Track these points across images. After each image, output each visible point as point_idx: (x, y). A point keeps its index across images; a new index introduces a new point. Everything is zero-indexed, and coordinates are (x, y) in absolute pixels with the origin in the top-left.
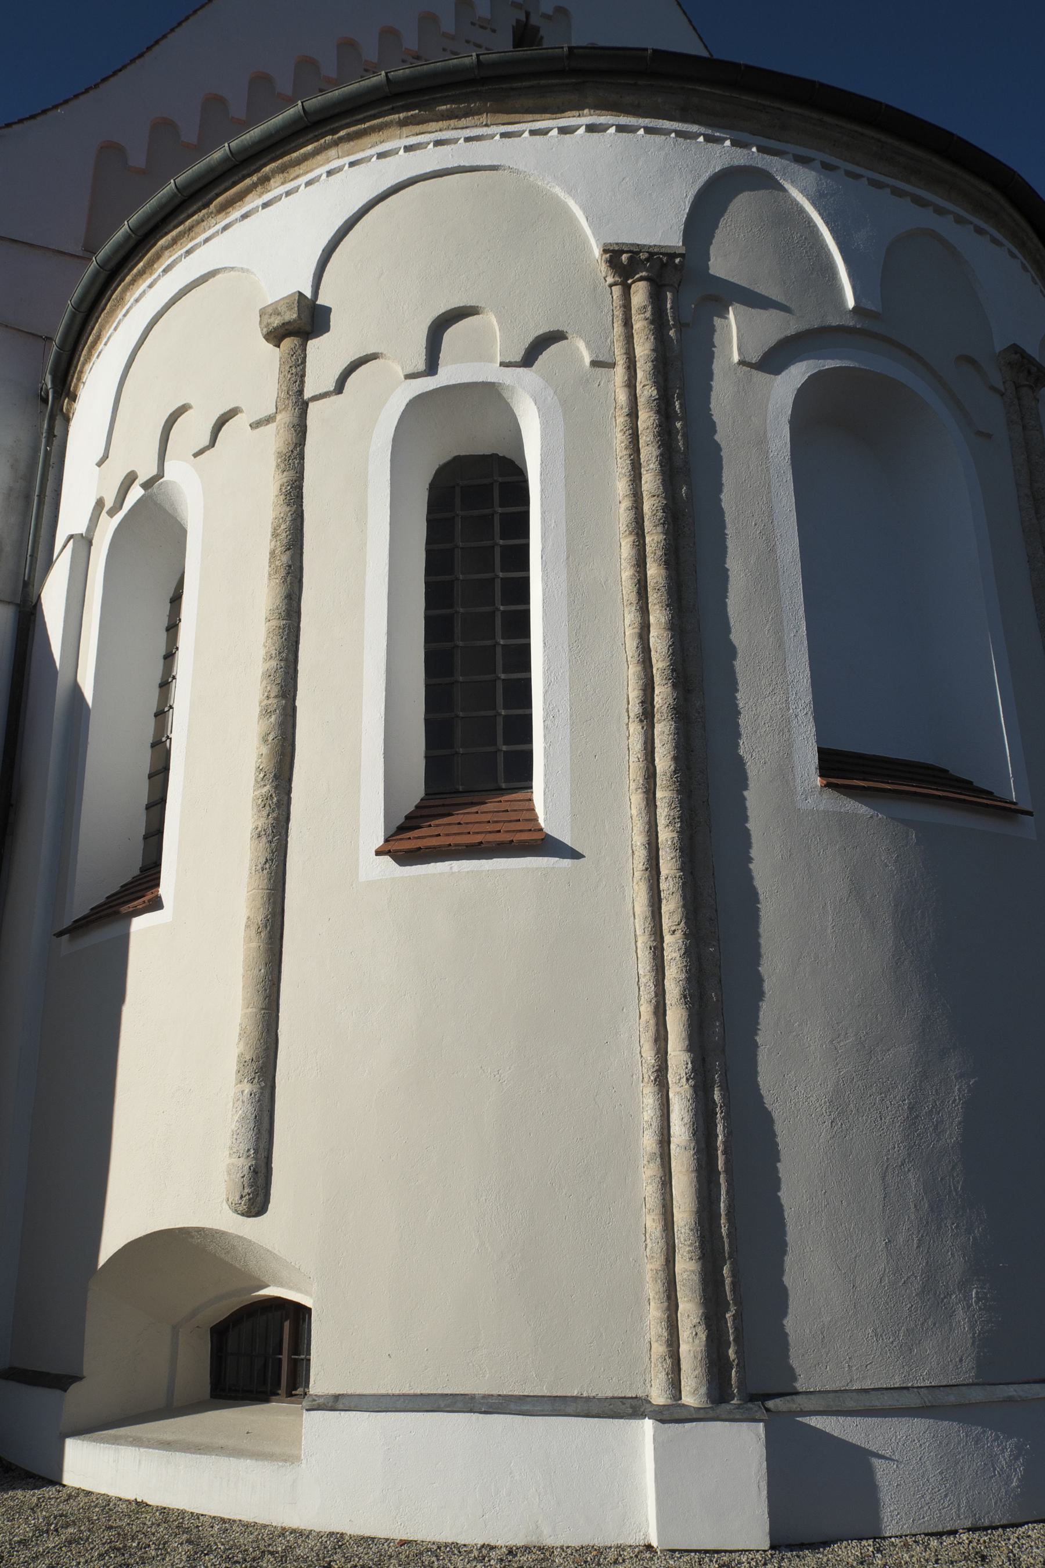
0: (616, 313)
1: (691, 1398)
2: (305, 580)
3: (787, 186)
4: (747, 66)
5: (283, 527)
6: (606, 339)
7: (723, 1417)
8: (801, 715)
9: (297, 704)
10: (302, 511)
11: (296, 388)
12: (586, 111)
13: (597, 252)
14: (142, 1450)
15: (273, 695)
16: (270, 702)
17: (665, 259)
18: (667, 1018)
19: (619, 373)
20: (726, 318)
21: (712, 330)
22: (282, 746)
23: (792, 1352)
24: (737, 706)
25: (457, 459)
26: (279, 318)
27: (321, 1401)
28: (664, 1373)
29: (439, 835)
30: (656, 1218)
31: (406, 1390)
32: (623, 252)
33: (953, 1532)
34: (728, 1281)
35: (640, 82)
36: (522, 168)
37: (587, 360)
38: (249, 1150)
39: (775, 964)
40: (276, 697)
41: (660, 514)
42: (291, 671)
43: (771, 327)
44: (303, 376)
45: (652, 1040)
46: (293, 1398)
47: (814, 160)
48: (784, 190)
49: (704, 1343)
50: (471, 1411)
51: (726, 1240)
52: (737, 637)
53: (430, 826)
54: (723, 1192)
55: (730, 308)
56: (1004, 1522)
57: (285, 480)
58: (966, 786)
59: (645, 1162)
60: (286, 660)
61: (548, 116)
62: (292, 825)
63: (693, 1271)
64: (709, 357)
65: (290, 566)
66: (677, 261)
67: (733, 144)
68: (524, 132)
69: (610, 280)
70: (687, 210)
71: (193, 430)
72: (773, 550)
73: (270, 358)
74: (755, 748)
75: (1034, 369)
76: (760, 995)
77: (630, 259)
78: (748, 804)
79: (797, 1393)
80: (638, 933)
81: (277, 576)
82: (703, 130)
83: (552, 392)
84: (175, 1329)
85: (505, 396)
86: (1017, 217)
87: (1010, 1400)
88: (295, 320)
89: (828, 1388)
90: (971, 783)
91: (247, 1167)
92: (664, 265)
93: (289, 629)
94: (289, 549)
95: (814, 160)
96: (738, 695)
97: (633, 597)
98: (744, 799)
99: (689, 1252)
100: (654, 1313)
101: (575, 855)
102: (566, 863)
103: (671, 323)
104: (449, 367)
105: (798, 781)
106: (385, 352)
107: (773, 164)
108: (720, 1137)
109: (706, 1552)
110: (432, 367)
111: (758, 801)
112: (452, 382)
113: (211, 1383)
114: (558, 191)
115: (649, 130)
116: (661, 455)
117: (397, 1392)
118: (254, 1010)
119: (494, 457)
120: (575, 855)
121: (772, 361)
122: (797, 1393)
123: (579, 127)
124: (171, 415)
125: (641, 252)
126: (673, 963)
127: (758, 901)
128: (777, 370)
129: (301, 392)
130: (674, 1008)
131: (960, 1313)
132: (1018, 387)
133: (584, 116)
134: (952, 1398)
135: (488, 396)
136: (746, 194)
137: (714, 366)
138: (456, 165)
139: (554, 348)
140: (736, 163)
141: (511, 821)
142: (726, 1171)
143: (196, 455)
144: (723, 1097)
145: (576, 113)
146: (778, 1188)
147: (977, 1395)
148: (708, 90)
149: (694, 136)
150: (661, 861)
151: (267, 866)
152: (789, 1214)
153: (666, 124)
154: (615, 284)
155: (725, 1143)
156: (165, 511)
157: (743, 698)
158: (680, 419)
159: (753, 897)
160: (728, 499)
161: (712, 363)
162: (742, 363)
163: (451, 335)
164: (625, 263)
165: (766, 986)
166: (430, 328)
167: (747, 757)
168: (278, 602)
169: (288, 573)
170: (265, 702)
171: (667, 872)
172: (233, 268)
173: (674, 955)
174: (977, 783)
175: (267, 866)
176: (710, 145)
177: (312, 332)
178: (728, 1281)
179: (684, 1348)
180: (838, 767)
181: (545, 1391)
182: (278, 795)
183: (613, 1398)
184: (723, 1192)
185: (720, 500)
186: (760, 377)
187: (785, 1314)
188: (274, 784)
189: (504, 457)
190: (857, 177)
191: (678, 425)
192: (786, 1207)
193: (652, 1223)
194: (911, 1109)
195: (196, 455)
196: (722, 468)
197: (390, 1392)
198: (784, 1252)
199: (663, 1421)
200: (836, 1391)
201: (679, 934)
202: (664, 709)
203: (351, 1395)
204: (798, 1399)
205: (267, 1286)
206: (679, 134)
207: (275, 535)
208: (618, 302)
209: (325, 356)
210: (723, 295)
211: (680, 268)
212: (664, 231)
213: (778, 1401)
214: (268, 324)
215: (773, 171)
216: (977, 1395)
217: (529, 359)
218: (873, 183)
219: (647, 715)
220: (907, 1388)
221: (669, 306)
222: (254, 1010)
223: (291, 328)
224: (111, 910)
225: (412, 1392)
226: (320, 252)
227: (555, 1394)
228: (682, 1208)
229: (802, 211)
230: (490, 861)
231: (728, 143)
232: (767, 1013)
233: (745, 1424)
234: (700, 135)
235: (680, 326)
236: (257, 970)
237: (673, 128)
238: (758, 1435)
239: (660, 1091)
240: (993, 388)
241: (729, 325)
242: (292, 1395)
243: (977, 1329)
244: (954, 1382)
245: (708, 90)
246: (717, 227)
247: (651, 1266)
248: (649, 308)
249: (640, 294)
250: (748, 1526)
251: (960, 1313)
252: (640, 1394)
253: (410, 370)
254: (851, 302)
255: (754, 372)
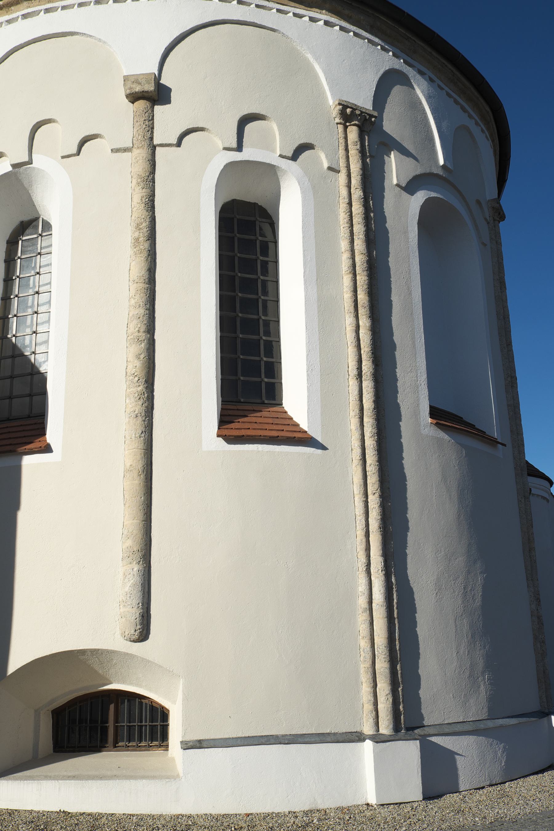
0: (341, 141)
1: (385, 729)
2: (157, 261)
3: (416, 87)
4: (408, 14)
5: (144, 224)
6: (336, 155)
7: (403, 738)
8: (423, 384)
9: (155, 338)
10: (155, 217)
11: (149, 135)
12: (324, 11)
13: (331, 101)
14: (60, 781)
15: (142, 330)
16: (140, 334)
17: (368, 117)
18: (370, 539)
19: (342, 177)
20: (390, 157)
21: (383, 163)
22: (149, 363)
23: (423, 706)
24: (396, 376)
25: (234, 201)
26: (140, 86)
27: (191, 744)
28: (372, 719)
29: (249, 429)
30: (367, 641)
31: (240, 735)
32: (348, 107)
33: (483, 788)
34: (399, 672)
35: (353, 4)
36: (289, 34)
37: (326, 165)
38: (139, 604)
39: (413, 514)
40: (144, 332)
41: (365, 264)
42: (152, 317)
43: (413, 168)
44: (153, 128)
45: (364, 549)
46: (118, 748)
47: (426, 74)
48: (414, 89)
49: (391, 703)
50: (280, 743)
51: (398, 652)
52: (397, 338)
53: (239, 422)
54: (397, 628)
55: (392, 152)
56: (500, 782)
57: (145, 194)
58: (472, 426)
59: (360, 612)
60: (149, 310)
61: (303, 7)
62: (155, 412)
63: (386, 668)
64: (383, 178)
65: (149, 251)
66: (373, 119)
67: (394, 55)
68: (289, 12)
69: (338, 120)
70: (374, 89)
71: (60, 137)
72: (410, 294)
73: (129, 111)
74: (405, 399)
75: (502, 213)
76: (407, 529)
77: (352, 112)
78: (402, 429)
79: (424, 726)
80: (355, 493)
81: (142, 255)
82: (380, 42)
83: (307, 180)
84: (37, 712)
85: (278, 174)
86: (495, 126)
87: (501, 726)
88: (151, 92)
89: (436, 723)
90: (474, 426)
91: (138, 614)
92: (366, 119)
93: (150, 290)
94: (149, 240)
95: (426, 74)
96: (397, 370)
97: (352, 309)
98: (400, 426)
99: (384, 658)
100: (366, 689)
101: (324, 448)
102: (319, 451)
103: (368, 154)
104: (249, 149)
105: (422, 419)
106: (210, 129)
107: (410, 72)
108: (395, 600)
109: (396, 804)
110: (239, 148)
111: (406, 427)
112: (251, 159)
113: (53, 744)
114: (309, 56)
115: (356, 34)
116: (366, 231)
117: (235, 736)
118: (138, 521)
119: (255, 204)
120: (324, 448)
121: (411, 187)
122: (424, 726)
123: (320, 20)
124: (37, 123)
125: (356, 109)
126: (374, 510)
127: (406, 481)
128: (412, 193)
129: (151, 139)
130: (375, 533)
131: (482, 687)
132: (494, 220)
133: (322, 14)
134: (482, 726)
135: (270, 171)
136: (396, 87)
137: (385, 184)
138: (252, 21)
139: (307, 153)
140: (395, 68)
141: (285, 425)
142: (398, 618)
143: (63, 157)
144: (396, 580)
145: (319, 11)
146: (416, 626)
147: (490, 724)
148: (385, 20)
149: (376, 44)
150: (367, 456)
151: (143, 435)
152: (421, 639)
153: (364, 33)
154: (340, 124)
155: (397, 603)
156: (22, 184)
157: (399, 372)
158: (373, 212)
159: (404, 478)
160: (392, 260)
161: (384, 182)
162: (398, 185)
163: (249, 128)
164: (348, 114)
165: (410, 524)
166: (238, 121)
167: (401, 403)
168: (143, 272)
169: (149, 255)
170: (137, 334)
171: (371, 462)
172: (91, 36)
173: (375, 506)
174: (476, 426)
175: (143, 435)
176: (383, 52)
177: (158, 100)
178: (399, 672)
179: (380, 706)
180: (434, 412)
181: (314, 732)
182: (147, 393)
183: (346, 733)
184: (397, 628)
185: (388, 261)
186: (405, 195)
187: (419, 688)
188: (145, 386)
189: (261, 206)
190: (442, 89)
191: (372, 215)
192: (419, 636)
193: (364, 644)
194: (464, 588)
195: (63, 157)
196: (389, 244)
197: (231, 736)
198: (419, 658)
199: (377, 742)
200: (439, 725)
201: (377, 495)
202: (369, 374)
203: (208, 740)
204: (425, 728)
205: (111, 683)
206: (370, 41)
207: (138, 227)
208: (341, 135)
209: (168, 120)
210: (389, 144)
211: (373, 124)
212: (364, 101)
213: (418, 730)
214: (130, 88)
215: (410, 76)
216: (490, 724)
217: (294, 157)
218: (448, 94)
219: (360, 376)
220: (464, 722)
221: (367, 144)
222: (138, 521)
223: (146, 95)
224: (8, 448)
225: (243, 736)
226: (164, 49)
227: (318, 732)
228: (381, 636)
229: (421, 103)
230: (279, 446)
231: (391, 53)
232: (411, 537)
233: (411, 741)
234: (379, 45)
235: (371, 156)
236: (139, 497)
237: (367, 36)
238: (417, 747)
239: (368, 576)
240: (486, 219)
241: (391, 161)
242: (115, 747)
243: (488, 693)
244: (481, 719)
245: (385, 20)
246: (386, 103)
247: (364, 666)
248: (359, 143)
249: (353, 133)
250: (413, 790)
251: (482, 687)
252: (359, 730)
253: (227, 145)
254: (441, 162)
255: (402, 191)
